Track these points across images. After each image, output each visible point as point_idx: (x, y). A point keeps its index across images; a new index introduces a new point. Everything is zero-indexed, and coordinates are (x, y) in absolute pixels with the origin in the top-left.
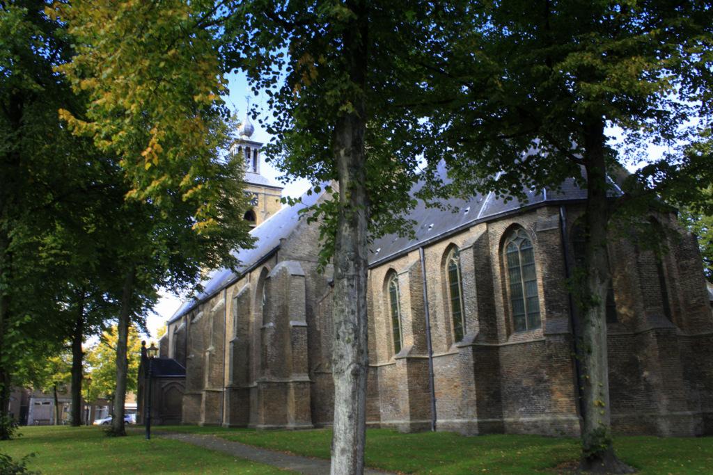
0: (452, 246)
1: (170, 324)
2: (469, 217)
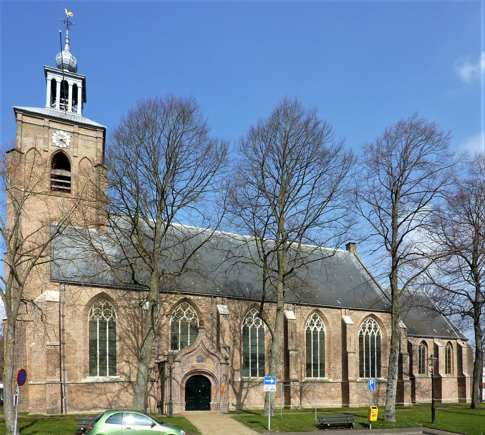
0: (185, 299)
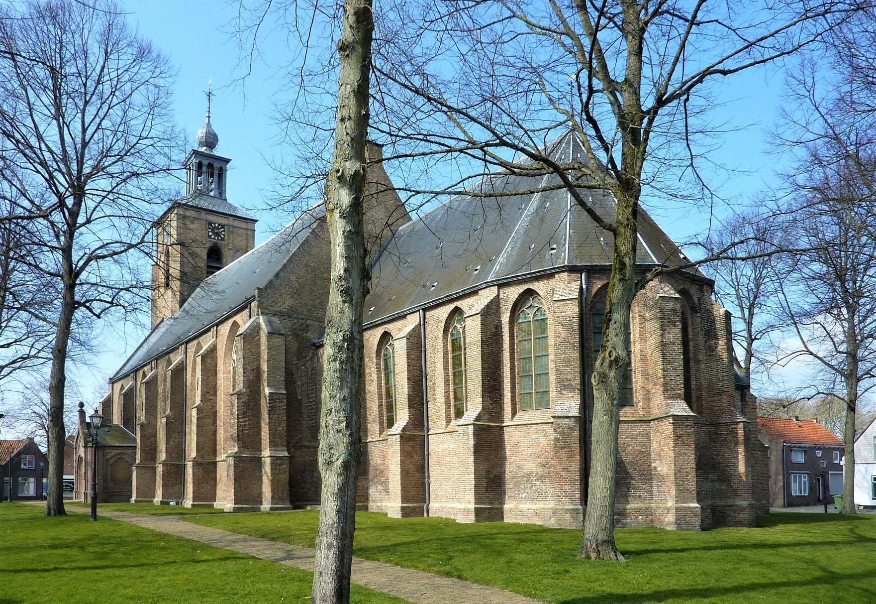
0: (457, 310)
1: (113, 381)
2: (478, 278)
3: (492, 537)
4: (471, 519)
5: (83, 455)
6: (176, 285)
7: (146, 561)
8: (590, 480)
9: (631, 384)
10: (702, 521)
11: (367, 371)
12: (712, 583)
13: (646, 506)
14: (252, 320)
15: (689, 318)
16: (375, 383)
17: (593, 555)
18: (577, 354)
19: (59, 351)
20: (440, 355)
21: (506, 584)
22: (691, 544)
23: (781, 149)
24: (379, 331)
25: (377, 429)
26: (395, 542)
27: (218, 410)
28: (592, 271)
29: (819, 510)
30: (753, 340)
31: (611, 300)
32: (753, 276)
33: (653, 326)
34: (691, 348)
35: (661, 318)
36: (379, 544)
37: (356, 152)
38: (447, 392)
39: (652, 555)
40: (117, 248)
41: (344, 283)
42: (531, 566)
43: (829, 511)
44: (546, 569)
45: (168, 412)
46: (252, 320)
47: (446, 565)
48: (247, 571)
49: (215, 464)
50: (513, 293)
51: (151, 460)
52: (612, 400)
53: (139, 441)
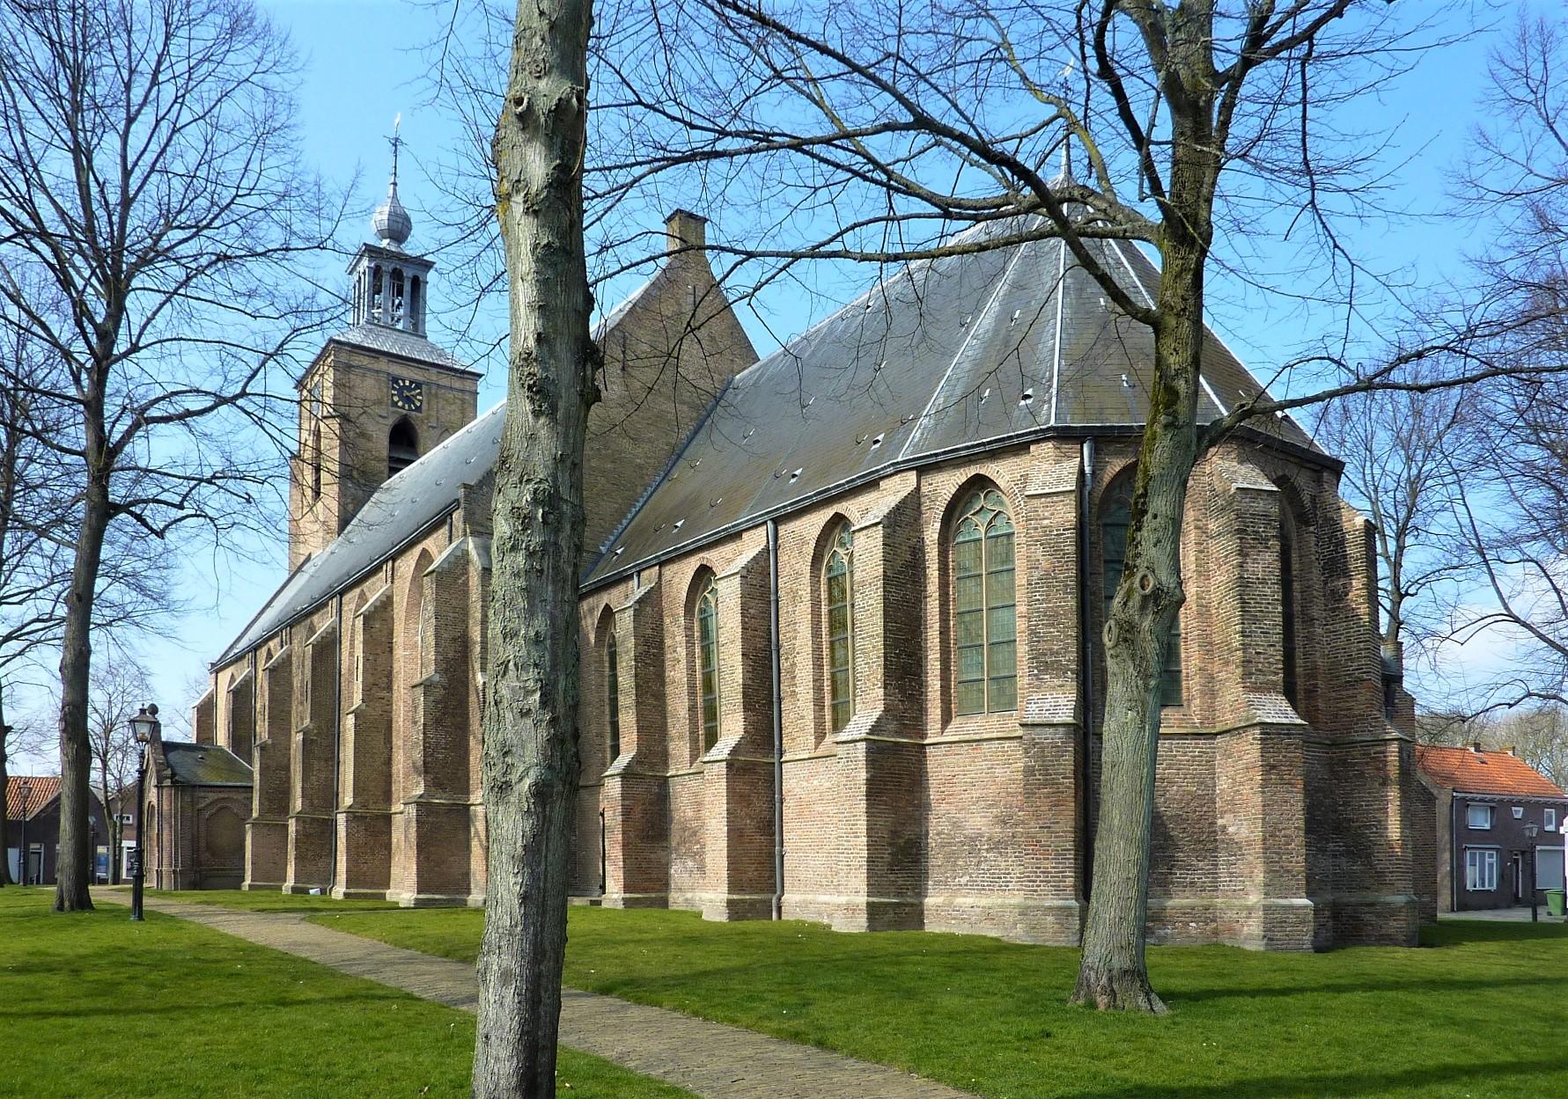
0: (839, 521)
1: (217, 668)
2: (878, 457)
3: (897, 959)
4: (859, 924)
5: (155, 802)
6: (331, 491)
7: (183, 1001)
8: (1097, 844)
9: (1178, 663)
10: (1316, 935)
11: (668, 642)
12: (1357, 1065)
13: (1205, 902)
14: (454, 545)
15: (1294, 536)
16: (683, 665)
17: (1102, 1001)
18: (1071, 602)
19: (80, 598)
20: (805, 608)
21: (917, 1062)
22: (1301, 979)
23: (1475, 209)
24: (690, 566)
25: (687, 753)
26: (701, 968)
27: (395, 718)
28: (1103, 439)
29: (1521, 915)
30: (1402, 597)
31: (1146, 470)
32: (1405, 475)
33: (1223, 547)
34: (1297, 595)
35: (1239, 531)
36: (668, 973)
37: (563, 57)
38: (818, 680)
39: (1223, 1001)
40: (194, 403)
41: (535, 369)
42: (972, 1023)
43: (1540, 919)
44: (1003, 1028)
45: (307, 721)
46: (454, 545)
47: (796, 1017)
48: (378, 1024)
49: (388, 819)
50: (946, 484)
51: (280, 813)
52: (1146, 677)
53: (257, 776)
